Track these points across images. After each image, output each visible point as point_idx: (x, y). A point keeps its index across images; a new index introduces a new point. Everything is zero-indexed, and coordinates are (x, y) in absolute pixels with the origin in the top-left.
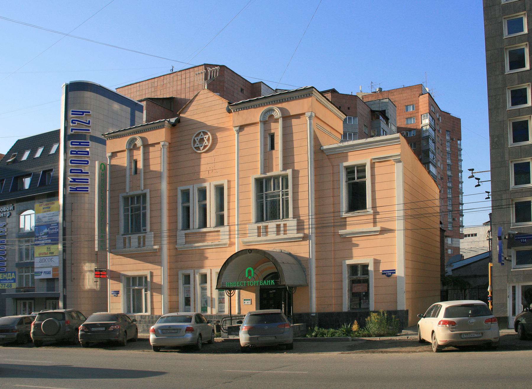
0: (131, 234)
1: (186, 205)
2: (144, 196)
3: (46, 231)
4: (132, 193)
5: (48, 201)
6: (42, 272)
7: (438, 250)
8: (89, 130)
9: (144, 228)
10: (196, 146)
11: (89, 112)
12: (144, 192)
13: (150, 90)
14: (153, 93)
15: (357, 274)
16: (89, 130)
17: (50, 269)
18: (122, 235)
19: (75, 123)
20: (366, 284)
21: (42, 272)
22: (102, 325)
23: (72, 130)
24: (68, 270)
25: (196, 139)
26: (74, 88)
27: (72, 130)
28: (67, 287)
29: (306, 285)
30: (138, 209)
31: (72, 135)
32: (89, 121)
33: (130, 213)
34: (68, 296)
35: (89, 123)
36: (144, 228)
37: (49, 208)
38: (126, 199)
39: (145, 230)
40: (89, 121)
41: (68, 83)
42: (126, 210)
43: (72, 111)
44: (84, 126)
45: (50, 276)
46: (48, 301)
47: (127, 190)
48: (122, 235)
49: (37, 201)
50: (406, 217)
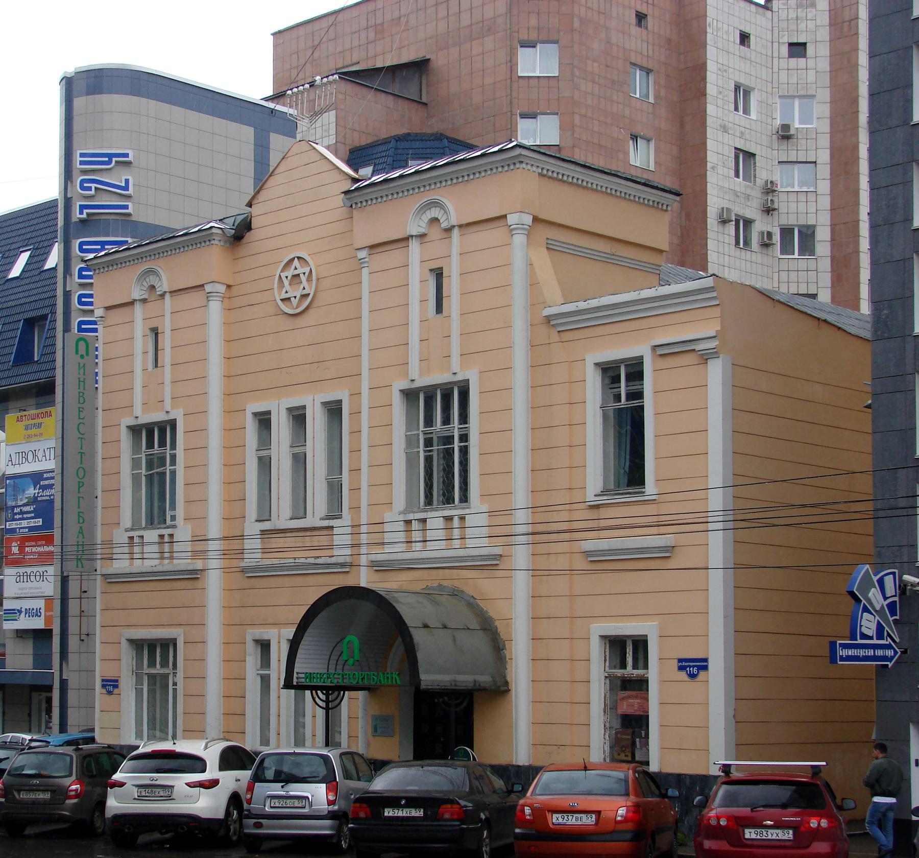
0: (144, 529)
1: (263, 453)
2: (173, 423)
3: (31, 491)
4: (145, 419)
5: (39, 406)
6: (20, 612)
7: (310, 631)
8: (126, 207)
9: (172, 513)
10: (284, 296)
11: (127, 155)
12: (171, 417)
13: (363, 35)
14: (371, 46)
15: (625, 668)
16: (126, 207)
17: (40, 604)
18: (127, 530)
19: (90, 189)
20: (476, 694)
21: (20, 612)
22: (413, 802)
23: (82, 207)
24: (73, 607)
25: (283, 275)
26: (85, 88)
27: (82, 207)
28: (71, 657)
29: (499, 690)
30: (162, 461)
31: (82, 221)
32: (127, 181)
33: (144, 471)
34: (71, 685)
35: (126, 188)
36: (172, 513)
37: (39, 426)
38: (135, 430)
39: (173, 518)
40: (127, 181)
41: (70, 69)
42: (136, 463)
43: (82, 155)
44: (114, 197)
45: (39, 623)
46: (35, 695)
47: (138, 410)
48: (127, 530)
49: (12, 404)
50: (744, 520)
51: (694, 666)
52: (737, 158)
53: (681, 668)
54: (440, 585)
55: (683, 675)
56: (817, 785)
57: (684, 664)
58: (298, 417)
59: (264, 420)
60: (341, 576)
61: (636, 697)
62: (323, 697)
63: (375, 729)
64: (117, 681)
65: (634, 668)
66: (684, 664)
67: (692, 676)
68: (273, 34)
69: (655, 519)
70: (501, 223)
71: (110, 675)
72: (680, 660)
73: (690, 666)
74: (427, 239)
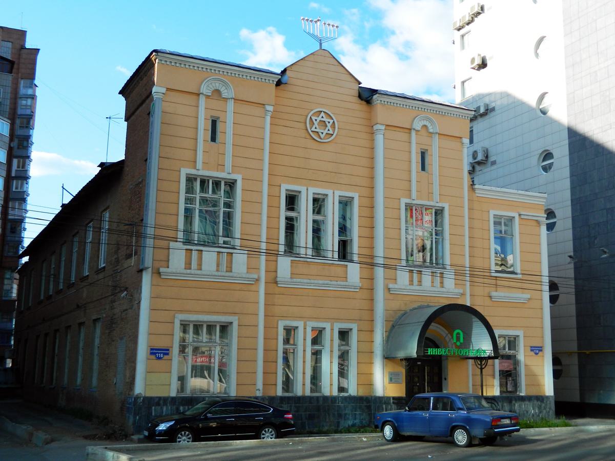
51: (161, 353)
52: (350, 197)
53: (532, 350)
54: (428, 305)
55: (532, 353)
56: (517, 392)
57: (154, 351)
58: (318, 204)
59: (292, 201)
60: (412, 289)
61: (506, 362)
62: (479, 363)
63: (391, 380)
64: (168, 350)
65: (509, 349)
66: (154, 351)
67: (536, 354)
68: (120, 93)
69: (525, 286)
70: (459, 140)
71: (161, 343)
72: (531, 347)
73: (159, 353)
74: (419, 133)
